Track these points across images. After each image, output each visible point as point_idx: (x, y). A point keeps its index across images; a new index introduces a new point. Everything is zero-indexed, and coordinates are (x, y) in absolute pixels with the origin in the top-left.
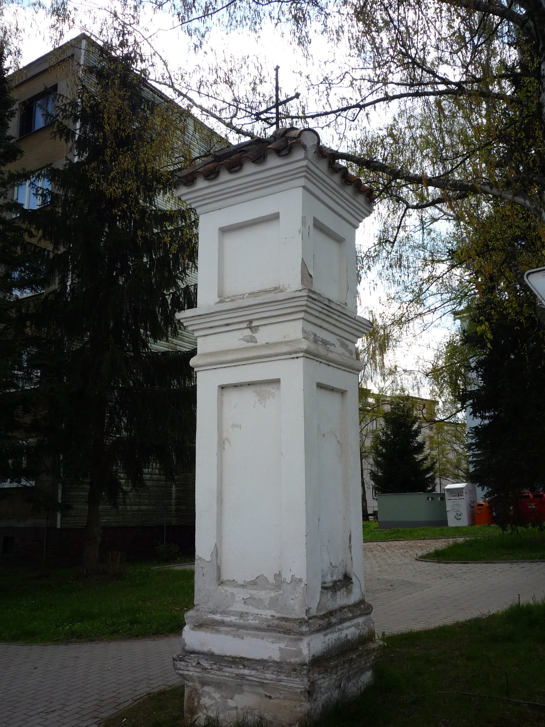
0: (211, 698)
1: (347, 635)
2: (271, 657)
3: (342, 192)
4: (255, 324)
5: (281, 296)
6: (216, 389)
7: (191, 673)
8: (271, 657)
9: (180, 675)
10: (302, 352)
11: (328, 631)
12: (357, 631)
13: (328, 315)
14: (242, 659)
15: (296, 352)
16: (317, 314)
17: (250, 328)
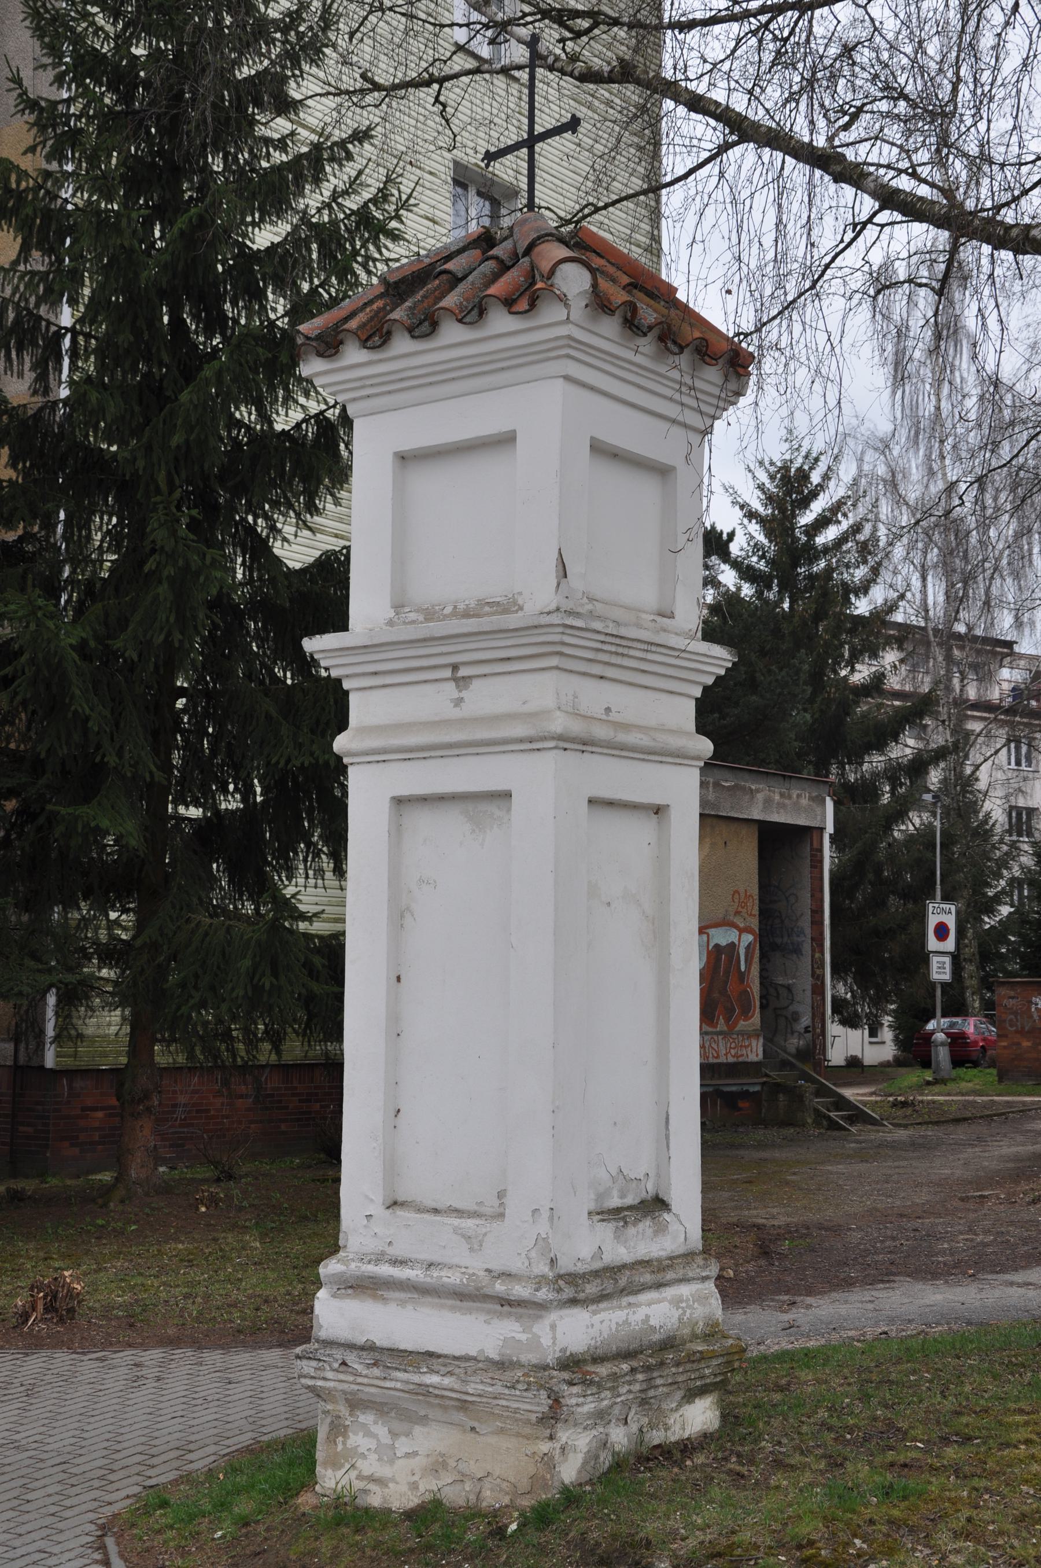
0: (368, 1434)
1: (648, 1317)
2: (482, 1351)
3: (662, 369)
4: (462, 672)
5: (513, 621)
6: (385, 806)
7: (331, 1384)
8: (482, 1351)
9: (308, 1387)
10: (553, 738)
11: (602, 1305)
12: (674, 1310)
13: (617, 654)
14: (430, 1354)
15: (544, 739)
16: (590, 655)
17: (455, 679)
